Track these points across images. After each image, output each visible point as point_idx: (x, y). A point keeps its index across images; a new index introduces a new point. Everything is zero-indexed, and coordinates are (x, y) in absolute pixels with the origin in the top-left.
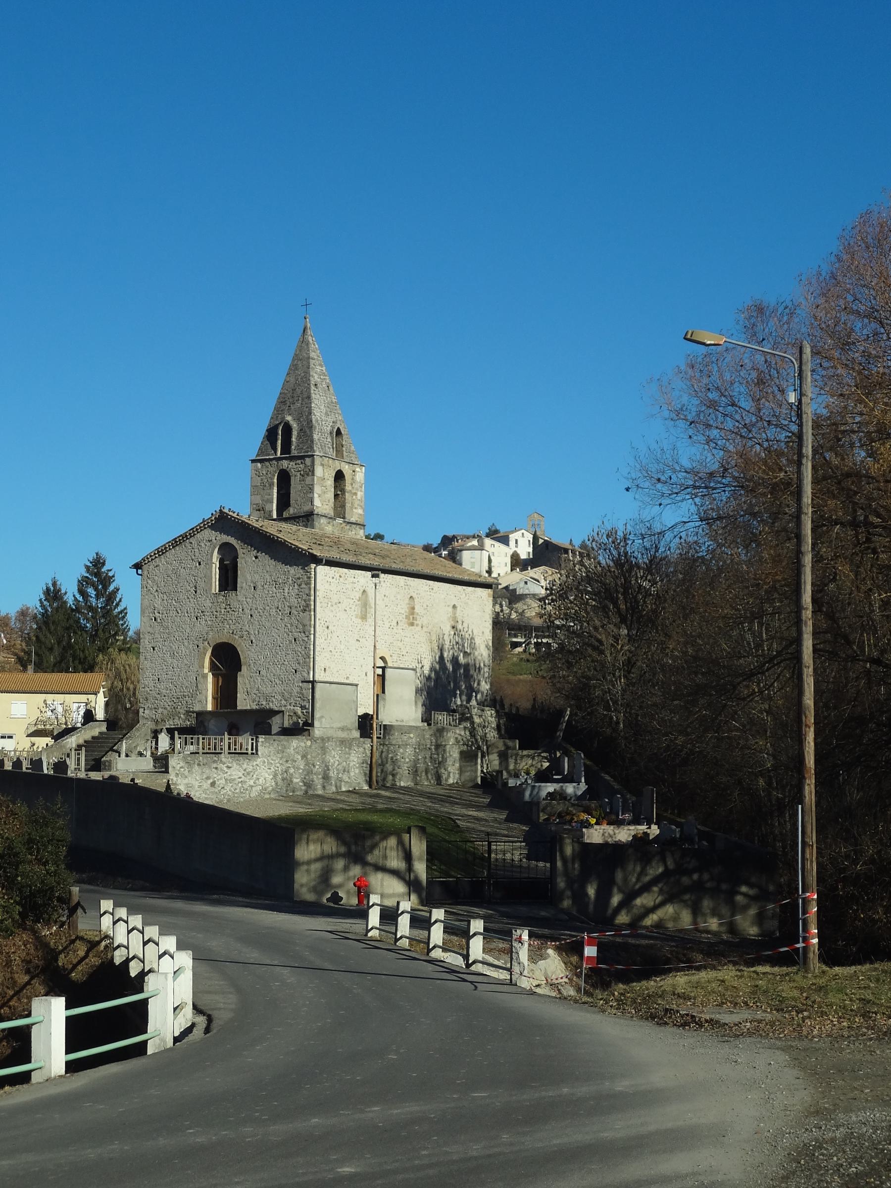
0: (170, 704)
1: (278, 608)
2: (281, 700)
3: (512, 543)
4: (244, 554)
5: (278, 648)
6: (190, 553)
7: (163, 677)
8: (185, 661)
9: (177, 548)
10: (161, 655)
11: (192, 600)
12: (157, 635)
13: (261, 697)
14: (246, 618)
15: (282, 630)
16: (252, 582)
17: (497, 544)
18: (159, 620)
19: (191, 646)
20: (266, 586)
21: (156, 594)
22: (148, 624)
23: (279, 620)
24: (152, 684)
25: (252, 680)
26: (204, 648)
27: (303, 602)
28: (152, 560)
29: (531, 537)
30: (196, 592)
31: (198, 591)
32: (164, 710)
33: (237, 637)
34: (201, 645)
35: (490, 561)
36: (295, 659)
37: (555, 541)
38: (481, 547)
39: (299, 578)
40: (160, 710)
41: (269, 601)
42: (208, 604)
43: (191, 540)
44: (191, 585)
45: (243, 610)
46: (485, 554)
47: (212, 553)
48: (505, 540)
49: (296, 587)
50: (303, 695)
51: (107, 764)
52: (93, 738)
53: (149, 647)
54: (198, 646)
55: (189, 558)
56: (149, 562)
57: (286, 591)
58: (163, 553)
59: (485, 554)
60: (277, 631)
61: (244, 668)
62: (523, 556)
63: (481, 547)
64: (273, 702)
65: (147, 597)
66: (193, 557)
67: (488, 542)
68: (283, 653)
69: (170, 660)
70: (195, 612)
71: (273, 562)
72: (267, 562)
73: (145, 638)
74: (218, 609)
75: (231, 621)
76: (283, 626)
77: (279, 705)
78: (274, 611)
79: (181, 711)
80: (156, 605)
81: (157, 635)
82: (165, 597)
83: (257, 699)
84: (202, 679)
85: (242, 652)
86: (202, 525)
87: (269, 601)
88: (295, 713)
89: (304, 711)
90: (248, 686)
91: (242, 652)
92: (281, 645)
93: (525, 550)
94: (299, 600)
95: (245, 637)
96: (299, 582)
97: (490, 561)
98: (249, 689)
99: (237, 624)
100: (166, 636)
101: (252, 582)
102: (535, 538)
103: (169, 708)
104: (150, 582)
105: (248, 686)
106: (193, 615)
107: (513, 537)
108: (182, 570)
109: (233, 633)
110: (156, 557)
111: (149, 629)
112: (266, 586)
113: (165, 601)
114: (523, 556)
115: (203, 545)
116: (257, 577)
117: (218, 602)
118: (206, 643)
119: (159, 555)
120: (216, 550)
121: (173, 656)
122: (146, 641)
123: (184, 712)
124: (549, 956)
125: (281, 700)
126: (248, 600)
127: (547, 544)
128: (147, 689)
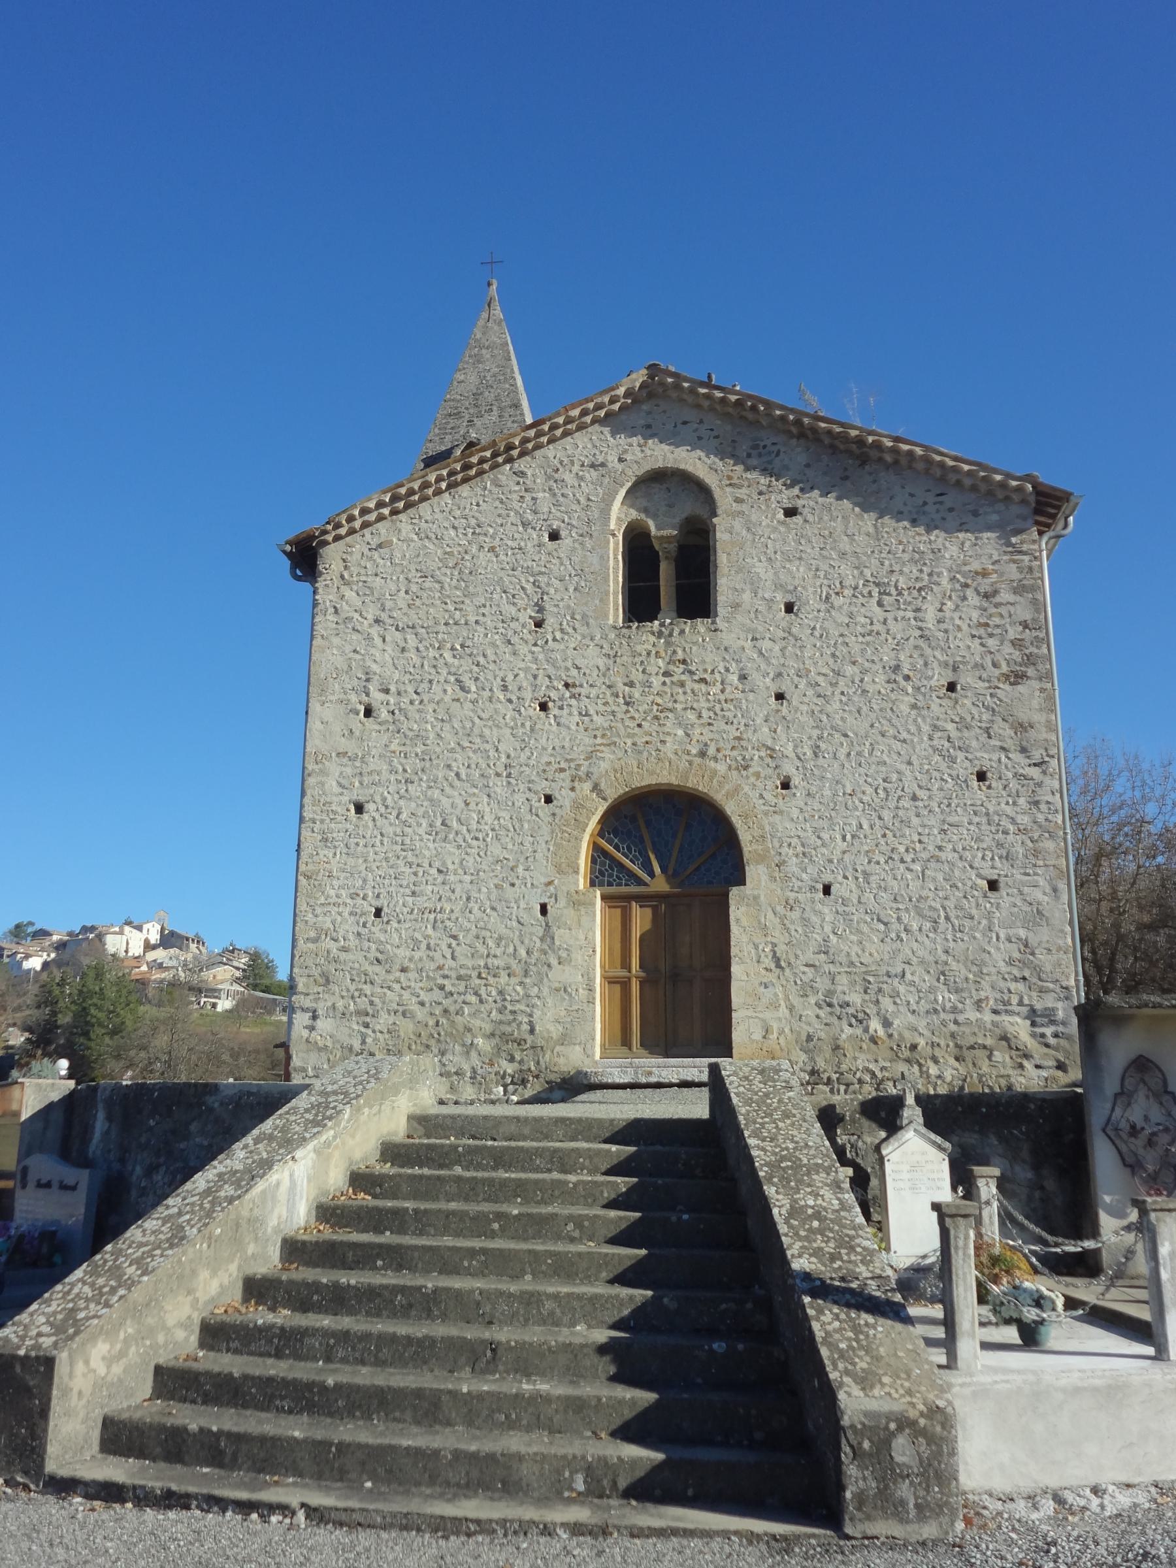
0: (424, 996)
1: (897, 668)
2: (932, 990)
3: (145, 931)
4: (738, 501)
5: (906, 803)
6: (516, 505)
7: (398, 903)
8: (496, 850)
9: (464, 490)
10: (389, 830)
11: (523, 649)
12: (374, 764)
13: (843, 980)
14: (761, 706)
15: (923, 746)
16: (779, 586)
17: (135, 931)
18: (384, 714)
19: (519, 799)
20: (838, 601)
21: (375, 631)
22: (337, 728)
23: (904, 708)
24: (349, 927)
25: (795, 915)
26: (578, 806)
27: (1008, 649)
28: (366, 525)
29: (159, 928)
30: (539, 624)
31: (550, 622)
32: (399, 1020)
33: (721, 768)
34: (564, 798)
35: (127, 943)
36: (988, 841)
37: (179, 931)
38: (121, 933)
39: (984, 574)
40: (384, 1020)
41: (856, 648)
42: (592, 658)
43: (520, 465)
44: (521, 603)
45: (743, 677)
46: (124, 938)
47: (609, 505)
48: (139, 928)
49: (973, 599)
50: (1038, 971)
51: (903, 1451)
52: (391, 1152)
53: (342, 803)
54: (548, 799)
55: (513, 517)
56: (352, 532)
57: (930, 615)
58: (408, 506)
59: (124, 938)
60: (897, 746)
61: (755, 873)
62: (153, 942)
63: (121, 933)
64: (894, 995)
65: (336, 641)
66: (529, 516)
67: (127, 929)
68: (933, 821)
69: (428, 848)
70: (535, 687)
71: (869, 521)
72: (838, 525)
73: (323, 772)
74: (637, 676)
75: (691, 716)
76: (926, 728)
77: (924, 1006)
78: (881, 678)
79: (476, 1023)
80: (374, 667)
81: (374, 764)
82: (412, 641)
83: (822, 984)
84: (570, 913)
85: (745, 816)
86: (575, 413)
87: (856, 648)
88: (1004, 1038)
89: (1048, 1031)
90: (779, 937)
91: (745, 816)
92: (921, 794)
93: (154, 938)
94: (992, 643)
95: (755, 767)
96: (985, 585)
97: (127, 943)
98: (781, 949)
99: (720, 725)
100: (412, 764)
101: (779, 586)
102: (163, 929)
103: (420, 1014)
104: (349, 594)
105: (779, 937)
106: (528, 695)
107: (145, 927)
108: (484, 557)
109: (703, 754)
110: (381, 518)
111: (344, 744)
112: (838, 601)
113: (412, 654)
114: (153, 942)
115: (569, 478)
116: (800, 571)
117: (635, 654)
118: (587, 786)
119: (394, 512)
120: (622, 493)
121: (442, 829)
122: (332, 784)
123: (488, 1028)
124: (593, 1456)
125: (932, 990)
126: (765, 645)
127: (172, 933)
128: (329, 944)
